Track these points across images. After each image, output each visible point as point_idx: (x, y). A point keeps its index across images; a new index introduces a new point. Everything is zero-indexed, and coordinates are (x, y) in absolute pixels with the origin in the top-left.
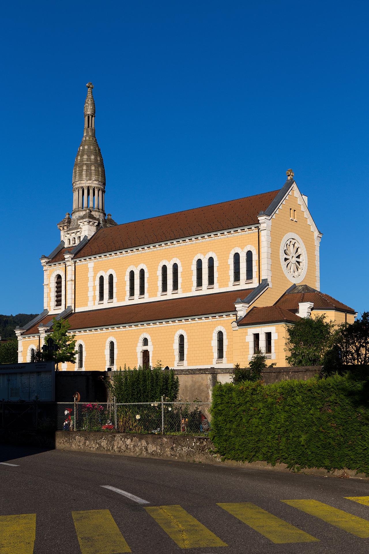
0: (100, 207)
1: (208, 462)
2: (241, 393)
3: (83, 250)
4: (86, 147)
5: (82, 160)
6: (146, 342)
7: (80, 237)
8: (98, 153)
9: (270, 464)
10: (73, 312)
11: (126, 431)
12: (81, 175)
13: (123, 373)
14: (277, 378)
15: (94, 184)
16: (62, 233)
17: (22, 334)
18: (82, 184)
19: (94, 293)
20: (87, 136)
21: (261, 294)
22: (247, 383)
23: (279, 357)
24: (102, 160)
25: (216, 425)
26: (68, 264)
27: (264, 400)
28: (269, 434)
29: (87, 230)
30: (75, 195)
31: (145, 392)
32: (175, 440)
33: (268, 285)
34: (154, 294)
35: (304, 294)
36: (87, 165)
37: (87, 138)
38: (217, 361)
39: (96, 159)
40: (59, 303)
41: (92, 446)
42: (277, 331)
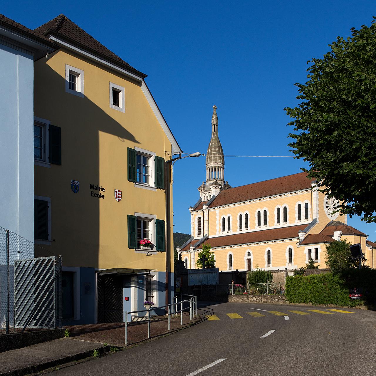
0: (222, 178)
1: (284, 304)
2: (296, 279)
3: (213, 203)
4: (213, 144)
5: (211, 151)
6: (249, 254)
7: (211, 195)
8: (220, 147)
9: (306, 304)
10: (208, 238)
11: (253, 294)
12: (211, 160)
13: (253, 272)
14: (313, 273)
15: (218, 165)
16: (201, 193)
17: (180, 251)
18: (211, 165)
19: (220, 227)
20: (213, 137)
21: (310, 230)
22: (298, 276)
23: (322, 263)
24: (222, 151)
25: (287, 291)
26: (205, 211)
27: (304, 281)
28: (306, 293)
29: (215, 192)
30: (208, 171)
31: (260, 280)
32: (272, 297)
33: (317, 222)
34: (253, 227)
35: (337, 226)
36: (214, 154)
37: (214, 138)
38: (288, 264)
39: (219, 150)
40: (200, 233)
41: (240, 300)
42: (321, 248)
